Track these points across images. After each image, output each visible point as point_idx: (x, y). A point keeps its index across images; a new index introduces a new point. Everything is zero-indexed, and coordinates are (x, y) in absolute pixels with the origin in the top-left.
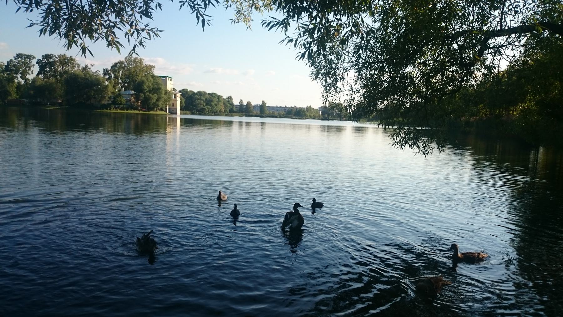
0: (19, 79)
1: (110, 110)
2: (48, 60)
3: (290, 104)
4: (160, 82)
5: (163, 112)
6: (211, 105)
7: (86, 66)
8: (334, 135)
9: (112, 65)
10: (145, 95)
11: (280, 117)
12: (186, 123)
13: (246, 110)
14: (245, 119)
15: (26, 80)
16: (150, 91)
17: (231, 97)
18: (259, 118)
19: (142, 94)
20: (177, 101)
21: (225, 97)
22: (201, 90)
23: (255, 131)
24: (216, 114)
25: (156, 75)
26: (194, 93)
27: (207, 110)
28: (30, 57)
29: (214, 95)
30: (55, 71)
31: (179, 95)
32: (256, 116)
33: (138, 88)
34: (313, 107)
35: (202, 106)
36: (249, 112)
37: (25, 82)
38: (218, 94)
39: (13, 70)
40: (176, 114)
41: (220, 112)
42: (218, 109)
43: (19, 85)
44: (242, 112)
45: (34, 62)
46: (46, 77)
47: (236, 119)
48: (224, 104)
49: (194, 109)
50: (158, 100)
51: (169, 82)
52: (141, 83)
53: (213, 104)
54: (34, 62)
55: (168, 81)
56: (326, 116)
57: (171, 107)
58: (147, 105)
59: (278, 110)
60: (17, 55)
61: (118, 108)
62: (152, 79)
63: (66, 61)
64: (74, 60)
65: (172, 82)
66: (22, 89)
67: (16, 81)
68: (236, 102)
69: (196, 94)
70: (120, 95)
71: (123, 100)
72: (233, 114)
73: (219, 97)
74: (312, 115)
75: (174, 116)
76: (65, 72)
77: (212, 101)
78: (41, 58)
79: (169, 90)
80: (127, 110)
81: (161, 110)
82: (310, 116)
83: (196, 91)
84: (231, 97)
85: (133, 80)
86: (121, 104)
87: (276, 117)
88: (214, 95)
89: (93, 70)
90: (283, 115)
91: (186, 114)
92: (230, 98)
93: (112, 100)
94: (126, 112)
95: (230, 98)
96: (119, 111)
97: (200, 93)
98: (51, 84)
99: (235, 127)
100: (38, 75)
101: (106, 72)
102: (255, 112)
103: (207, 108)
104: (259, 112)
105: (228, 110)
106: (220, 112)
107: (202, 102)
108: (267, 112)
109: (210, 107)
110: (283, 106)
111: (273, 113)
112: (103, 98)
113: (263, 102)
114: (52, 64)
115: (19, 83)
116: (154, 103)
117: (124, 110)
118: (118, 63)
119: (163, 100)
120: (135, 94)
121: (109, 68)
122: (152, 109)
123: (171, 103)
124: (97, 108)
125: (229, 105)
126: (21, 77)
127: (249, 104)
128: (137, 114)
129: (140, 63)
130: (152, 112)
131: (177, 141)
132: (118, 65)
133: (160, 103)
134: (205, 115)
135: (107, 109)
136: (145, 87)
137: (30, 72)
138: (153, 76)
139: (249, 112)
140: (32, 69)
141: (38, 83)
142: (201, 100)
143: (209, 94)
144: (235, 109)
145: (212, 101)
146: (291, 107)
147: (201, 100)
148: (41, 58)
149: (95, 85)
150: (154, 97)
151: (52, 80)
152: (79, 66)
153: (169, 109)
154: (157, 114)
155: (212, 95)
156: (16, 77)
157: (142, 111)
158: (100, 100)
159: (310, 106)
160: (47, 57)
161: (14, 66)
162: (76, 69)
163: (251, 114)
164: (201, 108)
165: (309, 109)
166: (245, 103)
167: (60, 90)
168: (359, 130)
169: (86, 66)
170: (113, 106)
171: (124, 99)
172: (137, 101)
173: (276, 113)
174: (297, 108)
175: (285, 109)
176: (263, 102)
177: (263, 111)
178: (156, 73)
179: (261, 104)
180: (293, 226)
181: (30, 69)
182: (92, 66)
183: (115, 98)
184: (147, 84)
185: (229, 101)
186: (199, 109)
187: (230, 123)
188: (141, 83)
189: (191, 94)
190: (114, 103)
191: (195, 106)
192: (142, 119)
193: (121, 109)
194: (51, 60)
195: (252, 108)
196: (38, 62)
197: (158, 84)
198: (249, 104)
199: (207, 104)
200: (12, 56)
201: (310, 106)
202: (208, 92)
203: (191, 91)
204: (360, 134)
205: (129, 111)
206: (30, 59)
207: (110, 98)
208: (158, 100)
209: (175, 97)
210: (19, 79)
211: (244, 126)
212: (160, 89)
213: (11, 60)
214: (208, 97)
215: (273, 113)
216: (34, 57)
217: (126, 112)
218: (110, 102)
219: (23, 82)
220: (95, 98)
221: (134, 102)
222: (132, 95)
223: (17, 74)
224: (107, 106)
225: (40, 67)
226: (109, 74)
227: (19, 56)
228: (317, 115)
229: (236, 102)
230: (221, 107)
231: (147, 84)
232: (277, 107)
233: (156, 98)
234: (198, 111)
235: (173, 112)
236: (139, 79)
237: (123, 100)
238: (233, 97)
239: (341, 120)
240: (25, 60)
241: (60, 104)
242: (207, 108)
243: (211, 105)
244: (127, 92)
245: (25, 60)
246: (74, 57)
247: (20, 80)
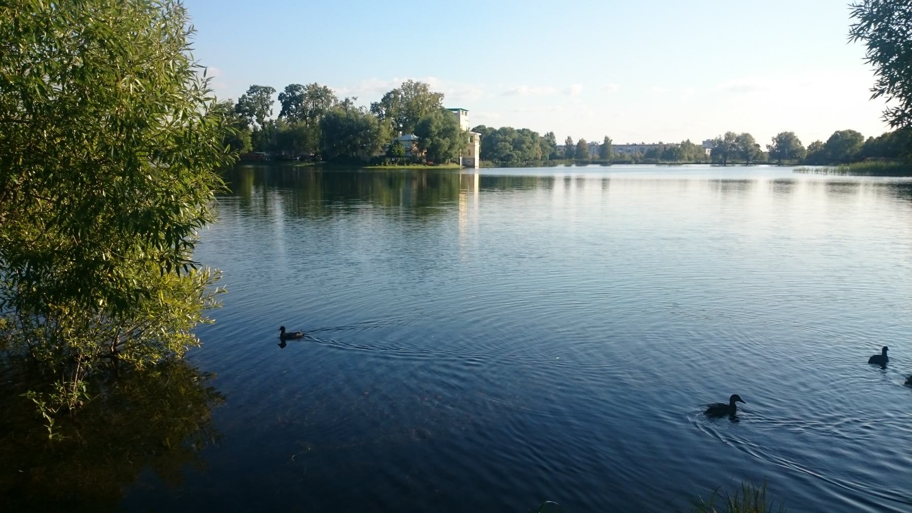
0: (254, 125)
1: (385, 165)
2: (293, 94)
3: (651, 139)
4: (454, 119)
5: (455, 166)
6: (521, 149)
7: (347, 100)
8: (734, 197)
9: (382, 97)
10: (432, 140)
11: (637, 163)
12: (487, 183)
13: (577, 154)
14: (575, 171)
15: (263, 124)
16: (439, 134)
17: (552, 134)
18: (597, 166)
19: (428, 139)
20: (474, 146)
21: (542, 135)
22: (506, 125)
23: (592, 190)
24: (530, 162)
25: (447, 107)
26: (494, 132)
27: (516, 157)
28: (268, 90)
29: (526, 133)
30: (304, 110)
31: (477, 136)
32: (594, 163)
33: (423, 130)
34: (691, 141)
35: (508, 151)
36: (581, 157)
37: (263, 127)
38: (533, 130)
39: (247, 111)
40: (473, 167)
41: (536, 158)
42: (532, 156)
43: (255, 134)
44: (570, 157)
45: (274, 97)
46: (291, 119)
47: (559, 172)
48: (541, 145)
49: (496, 157)
50: (450, 148)
51: (463, 117)
52: (426, 124)
53: (524, 146)
54: (274, 97)
55: (461, 116)
56: (721, 157)
57: (466, 156)
58: (435, 155)
59: (629, 151)
60: (251, 88)
61: (396, 161)
62: (442, 115)
63: (319, 94)
64: (330, 92)
65: (467, 118)
66: (259, 138)
67: (250, 126)
68: (560, 141)
69: (499, 132)
70: (397, 142)
71: (402, 149)
72: (556, 161)
73: (534, 135)
74: (692, 156)
75: (469, 172)
76: (320, 111)
77: (523, 142)
78: (283, 91)
79: (464, 129)
80: (408, 164)
81: (453, 162)
82: (689, 159)
83: (497, 128)
84: (552, 134)
85: (414, 119)
86: (399, 156)
87: (630, 163)
88: (526, 133)
89: (356, 105)
90: (641, 158)
91: (487, 166)
92: (551, 135)
93: (387, 150)
94: (407, 167)
95: (551, 135)
96: (397, 167)
97: (504, 131)
98: (300, 129)
99: (559, 187)
100: (280, 116)
101: (375, 108)
102: (590, 156)
103: (516, 154)
104: (597, 156)
105: (547, 155)
106: (536, 158)
107: (508, 144)
108: (612, 156)
109: (520, 153)
110: (638, 142)
111: (622, 156)
112: (375, 147)
113: (607, 139)
114: (300, 99)
115: (255, 128)
116: (446, 152)
117: (403, 164)
118: (392, 92)
119: (457, 146)
120: (419, 140)
121: (379, 101)
122: (443, 161)
123: (466, 150)
124: (366, 164)
125: (549, 147)
126: (257, 121)
127: (582, 143)
128: (421, 171)
129: (424, 91)
130: (441, 166)
131: (474, 215)
132: (392, 96)
133: (453, 152)
134: (513, 165)
135: (380, 164)
136: (433, 128)
137: (269, 112)
138: (443, 110)
139: (581, 157)
140: (271, 107)
141: (282, 129)
142: (505, 141)
143: (518, 131)
144: (558, 154)
145: (523, 142)
146: (654, 145)
147: (505, 141)
148: (283, 91)
149: (361, 130)
150: (445, 142)
151: (301, 124)
152: (336, 101)
153: (463, 159)
154: (448, 170)
155: (522, 132)
156: (251, 120)
157: (428, 164)
158: (371, 152)
159: (688, 141)
160: (292, 88)
161: (248, 104)
162: (332, 105)
163: (585, 160)
164: (513, 155)
165: (687, 145)
166: (575, 142)
167: (313, 140)
168: (783, 185)
169: (347, 100)
170: (388, 160)
171: (403, 148)
172: (421, 151)
173: (627, 156)
174: (665, 146)
175: (642, 147)
176: (607, 139)
177: (606, 155)
178: (446, 104)
179: (602, 143)
180: (725, 411)
181: (268, 108)
182: (355, 99)
183: (391, 147)
184: (436, 124)
185: (548, 141)
186: (502, 155)
187: (549, 182)
188: (426, 124)
189: (490, 132)
190: (390, 154)
191: (496, 151)
192: (428, 180)
193: (400, 164)
194: (298, 93)
195: (587, 151)
196: (281, 97)
197: (451, 123)
198: (582, 143)
199: (515, 147)
200: (243, 90)
201: (688, 141)
202: (516, 128)
203: (491, 129)
204: (785, 195)
205: (411, 167)
206: (268, 93)
207: (384, 147)
208: (450, 148)
209: (471, 141)
210: (254, 125)
211: (573, 184)
212: (453, 129)
213: (244, 96)
214: (516, 135)
215: (622, 156)
216: (274, 90)
217: (407, 167)
218: (384, 154)
219: (259, 127)
220: (363, 148)
221: (416, 152)
222: (413, 141)
223: (251, 116)
224: (379, 160)
225: (283, 104)
226: (378, 110)
227: (254, 89)
228: (701, 156)
229: (560, 141)
230: (537, 151)
231: (436, 124)
232: (628, 145)
233: (448, 144)
234: (502, 159)
235: (469, 165)
236: (422, 117)
237: (402, 149)
238: (555, 134)
239: (747, 164)
240: (261, 94)
241: (314, 159)
242: (516, 154)
243: (521, 149)
244: (407, 137)
245: (261, 94)
246: (329, 88)
247: (256, 124)
